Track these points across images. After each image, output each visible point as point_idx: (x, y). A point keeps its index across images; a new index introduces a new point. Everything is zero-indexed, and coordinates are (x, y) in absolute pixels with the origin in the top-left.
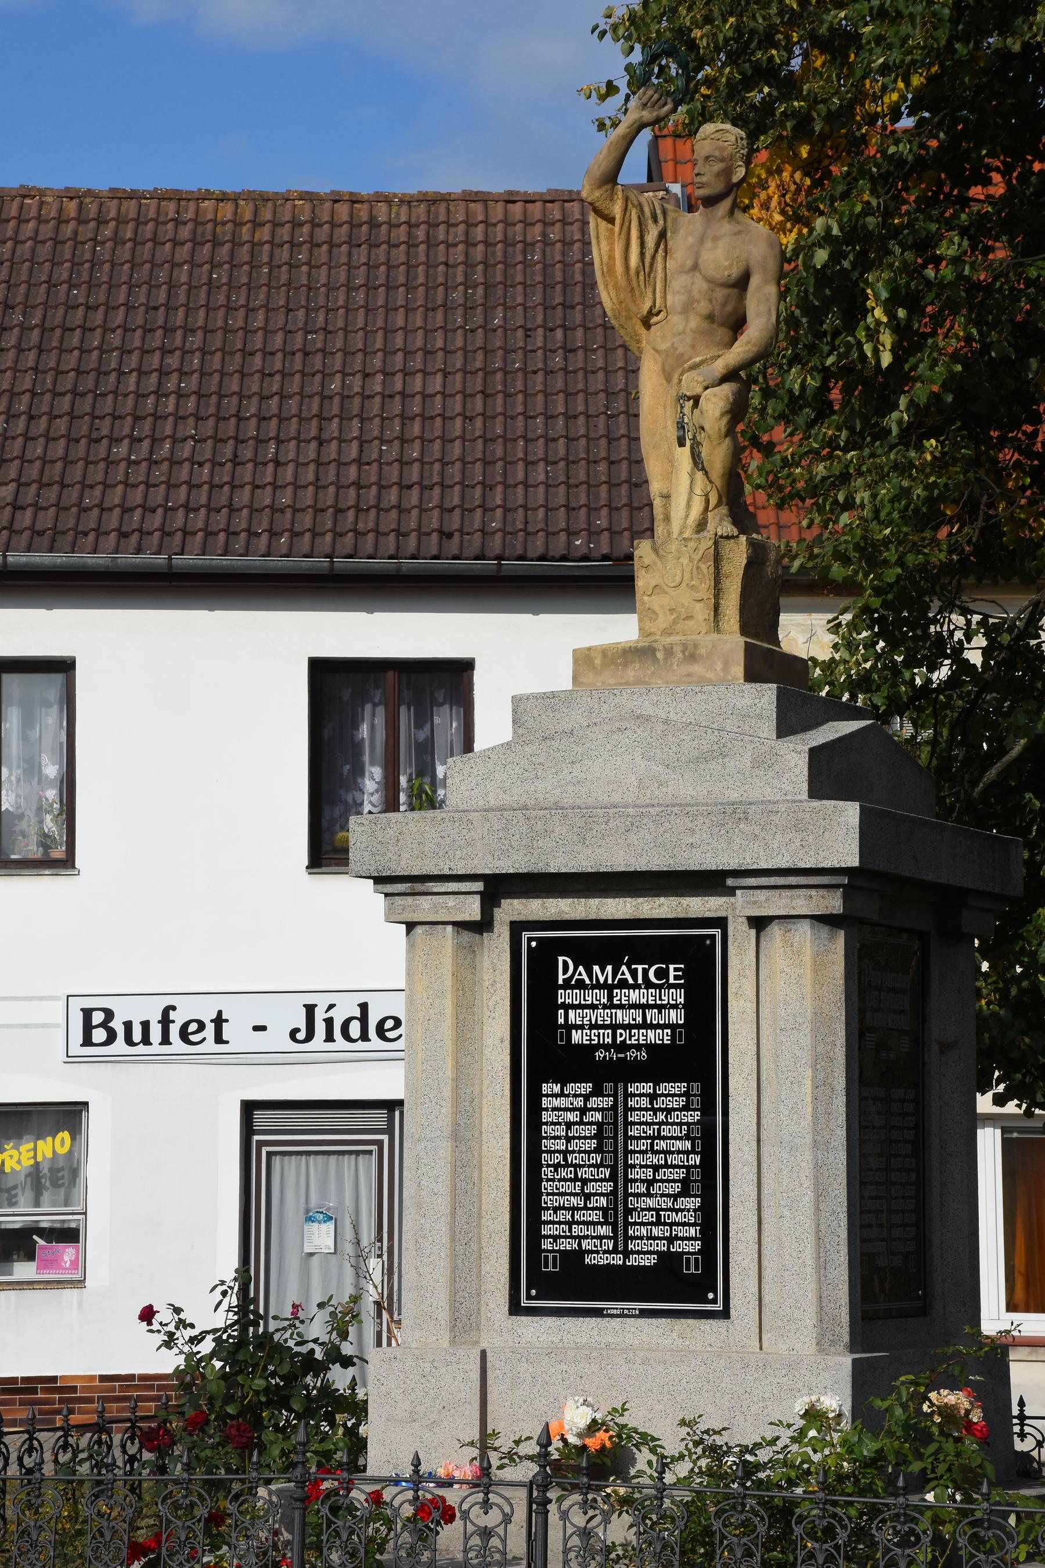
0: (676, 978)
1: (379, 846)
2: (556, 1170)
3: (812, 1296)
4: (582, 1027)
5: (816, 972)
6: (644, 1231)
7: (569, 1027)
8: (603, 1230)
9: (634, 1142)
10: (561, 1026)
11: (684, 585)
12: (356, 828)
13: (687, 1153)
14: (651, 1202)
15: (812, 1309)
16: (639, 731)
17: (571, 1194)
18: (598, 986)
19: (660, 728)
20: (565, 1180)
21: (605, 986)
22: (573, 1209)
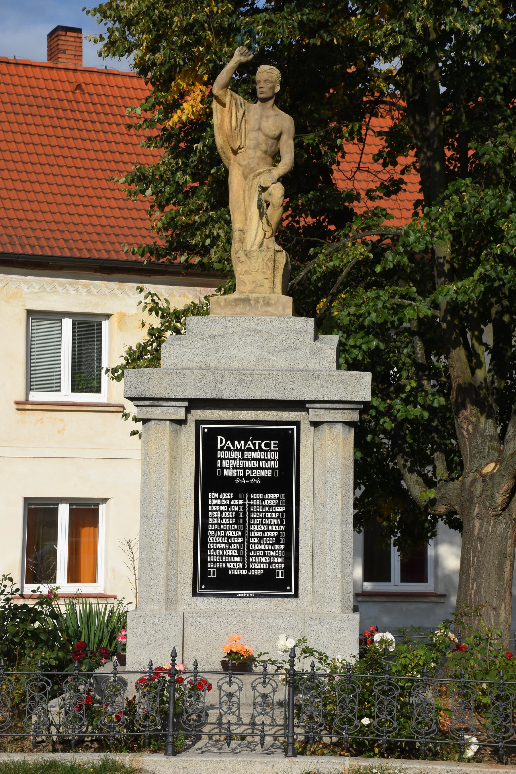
0: (274, 447)
1: (139, 384)
2: (215, 532)
3: (339, 588)
4: (229, 468)
5: (343, 446)
6: (257, 559)
7: (223, 468)
8: (238, 559)
9: (253, 520)
10: (219, 468)
11: (259, 271)
12: (128, 375)
13: (279, 525)
14: (261, 547)
15: (339, 594)
16: (256, 336)
17: (222, 543)
18: (237, 450)
19: (266, 335)
20: (219, 536)
21: (240, 450)
22: (223, 549)
